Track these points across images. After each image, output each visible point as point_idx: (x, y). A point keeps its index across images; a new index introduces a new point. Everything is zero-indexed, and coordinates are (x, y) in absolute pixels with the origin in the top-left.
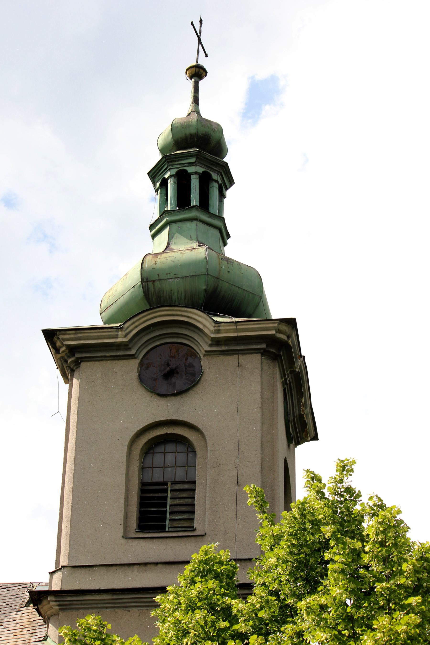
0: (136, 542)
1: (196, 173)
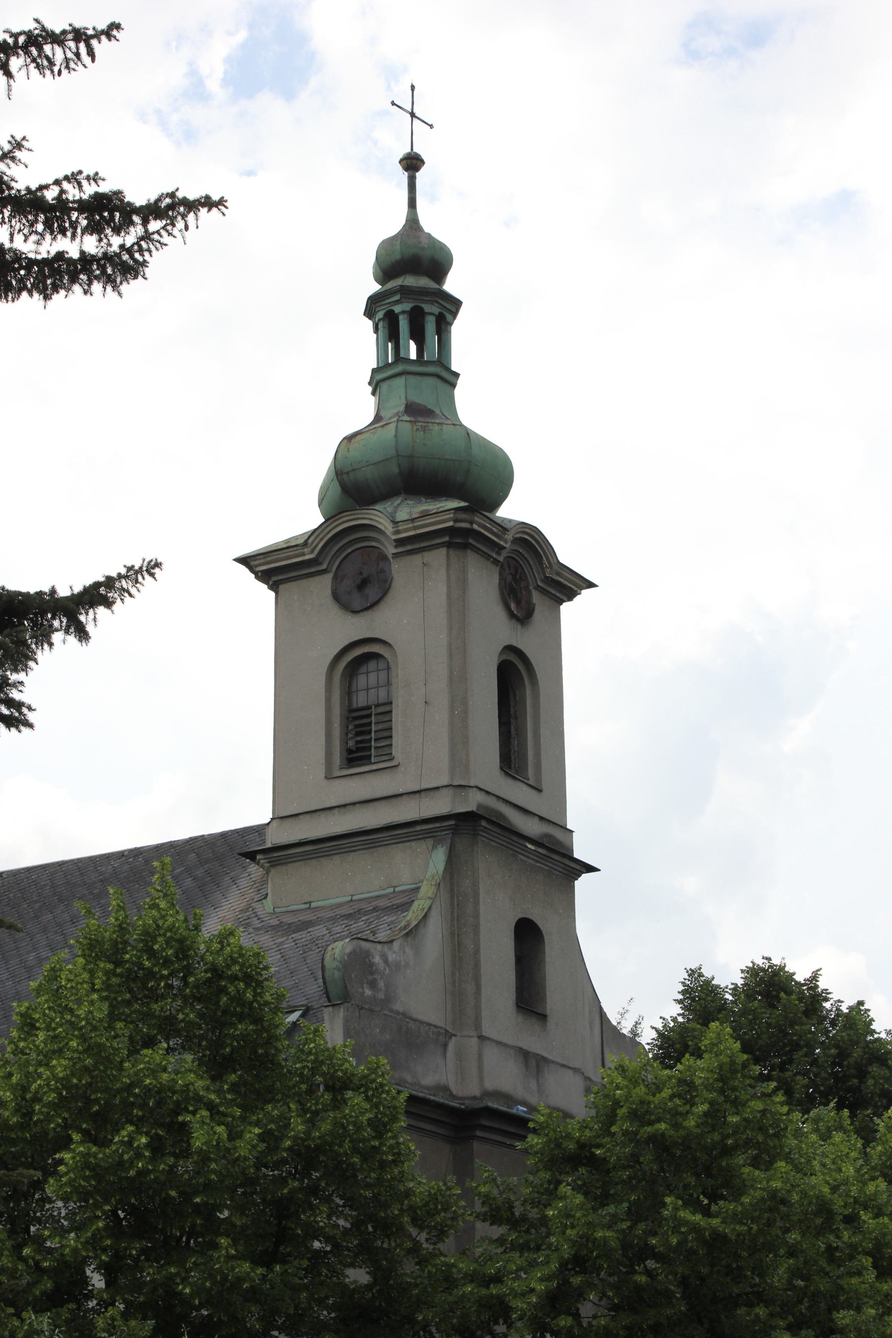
0: (343, 782)
1: (403, 312)
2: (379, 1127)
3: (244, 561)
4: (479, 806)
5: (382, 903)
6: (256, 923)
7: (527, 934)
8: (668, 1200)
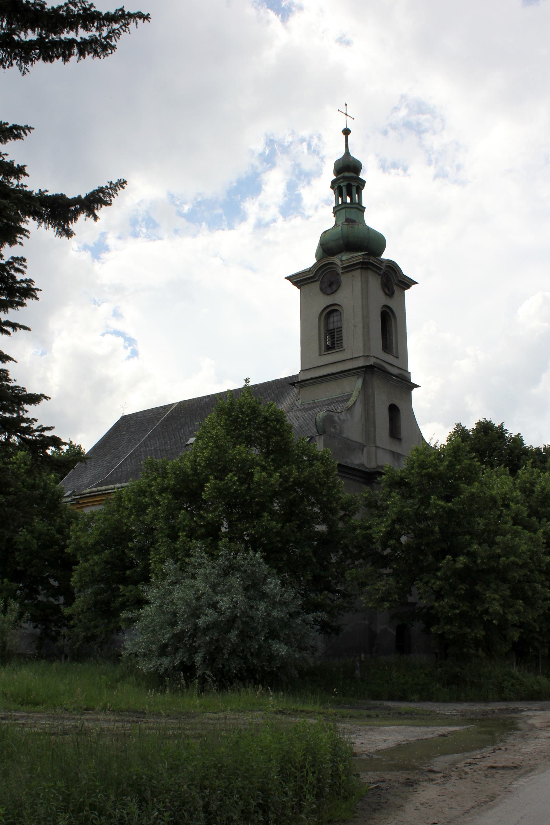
1: (344, 186)
2: (327, 474)
3: (288, 278)
4: (374, 363)
5: (340, 399)
6: (295, 408)
7: (394, 410)
8: (432, 497)
